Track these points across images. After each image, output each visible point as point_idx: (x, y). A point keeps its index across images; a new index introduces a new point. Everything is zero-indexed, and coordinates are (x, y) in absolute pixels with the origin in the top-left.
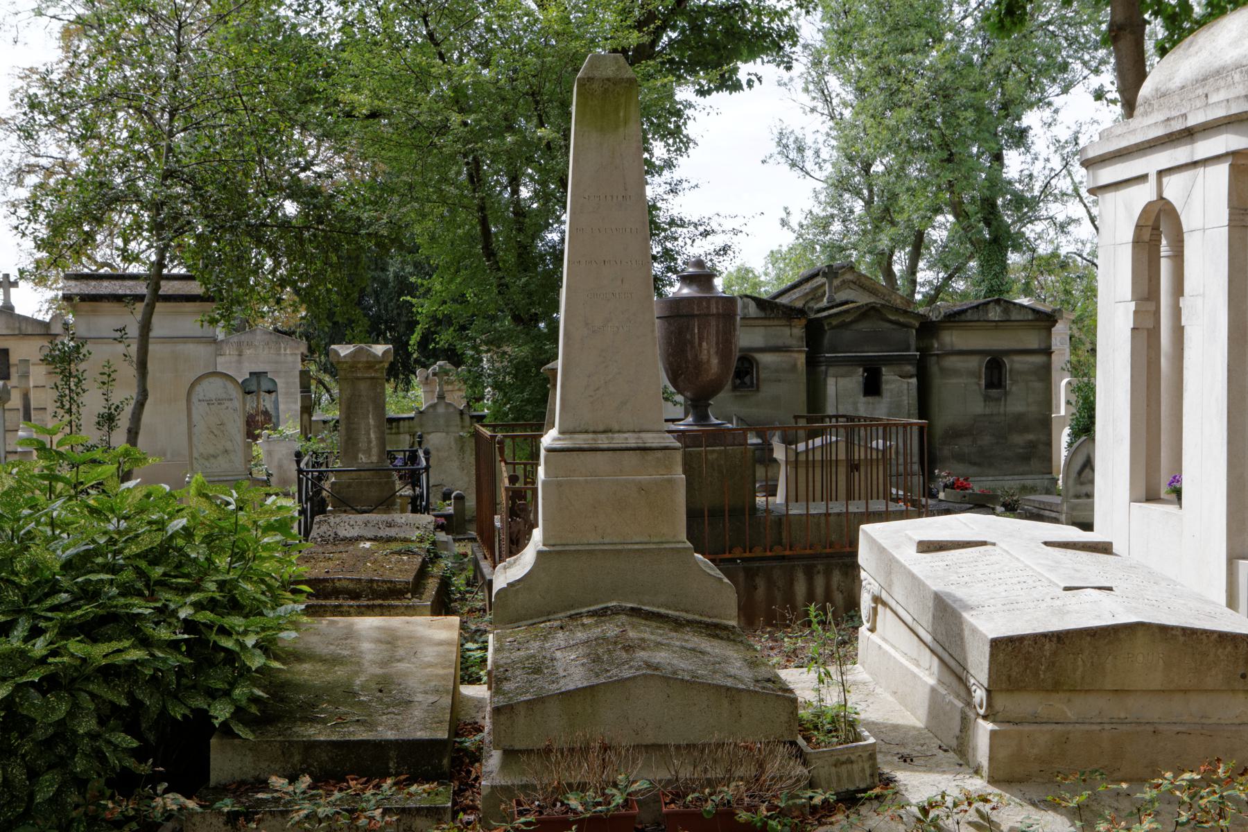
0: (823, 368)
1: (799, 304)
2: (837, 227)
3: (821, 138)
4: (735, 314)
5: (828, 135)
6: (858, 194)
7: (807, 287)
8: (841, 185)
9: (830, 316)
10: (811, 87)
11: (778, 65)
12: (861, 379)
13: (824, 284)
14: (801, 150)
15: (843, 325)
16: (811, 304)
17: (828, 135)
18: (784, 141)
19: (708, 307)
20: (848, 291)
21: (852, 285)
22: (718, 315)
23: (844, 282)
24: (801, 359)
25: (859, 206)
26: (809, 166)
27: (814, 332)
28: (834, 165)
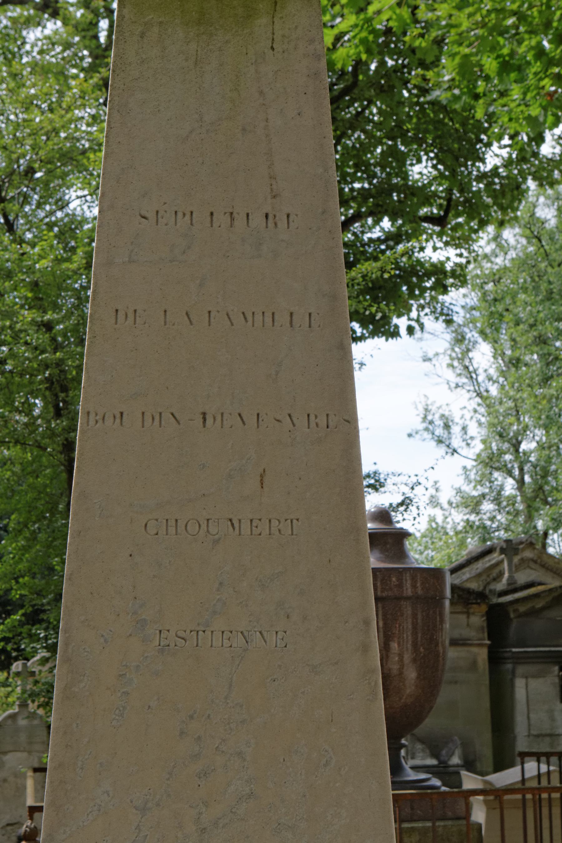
0: (509, 666)
1: (474, 586)
2: (487, 506)
3: (468, 416)
4: (443, 598)
5: (475, 411)
6: (510, 473)
7: (480, 566)
8: (490, 462)
9: (517, 601)
10: (456, 363)
11: (437, 319)
12: (557, 680)
13: (502, 561)
14: (447, 427)
15: (534, 613)
16: (492, 587)
17: (475, 411)
18: (430, 418)
19: (400, 586)
20: (528, 571)
21: (532, 565)
22: (415, 599)
23: (522, 560)
24: (482, 654)
25: (509, 487)
26: (456, 442)
27: (498, 621)
28: (484, 442)
